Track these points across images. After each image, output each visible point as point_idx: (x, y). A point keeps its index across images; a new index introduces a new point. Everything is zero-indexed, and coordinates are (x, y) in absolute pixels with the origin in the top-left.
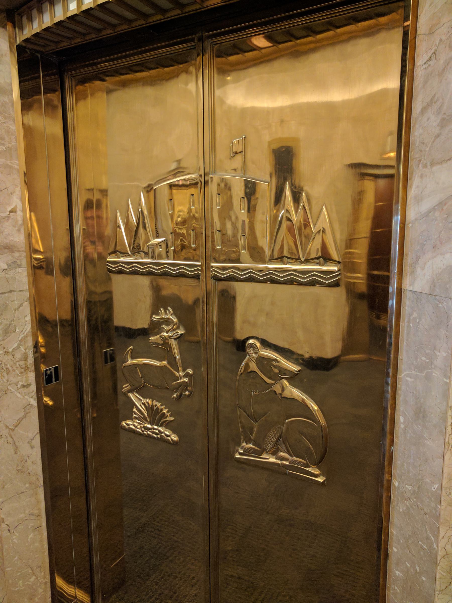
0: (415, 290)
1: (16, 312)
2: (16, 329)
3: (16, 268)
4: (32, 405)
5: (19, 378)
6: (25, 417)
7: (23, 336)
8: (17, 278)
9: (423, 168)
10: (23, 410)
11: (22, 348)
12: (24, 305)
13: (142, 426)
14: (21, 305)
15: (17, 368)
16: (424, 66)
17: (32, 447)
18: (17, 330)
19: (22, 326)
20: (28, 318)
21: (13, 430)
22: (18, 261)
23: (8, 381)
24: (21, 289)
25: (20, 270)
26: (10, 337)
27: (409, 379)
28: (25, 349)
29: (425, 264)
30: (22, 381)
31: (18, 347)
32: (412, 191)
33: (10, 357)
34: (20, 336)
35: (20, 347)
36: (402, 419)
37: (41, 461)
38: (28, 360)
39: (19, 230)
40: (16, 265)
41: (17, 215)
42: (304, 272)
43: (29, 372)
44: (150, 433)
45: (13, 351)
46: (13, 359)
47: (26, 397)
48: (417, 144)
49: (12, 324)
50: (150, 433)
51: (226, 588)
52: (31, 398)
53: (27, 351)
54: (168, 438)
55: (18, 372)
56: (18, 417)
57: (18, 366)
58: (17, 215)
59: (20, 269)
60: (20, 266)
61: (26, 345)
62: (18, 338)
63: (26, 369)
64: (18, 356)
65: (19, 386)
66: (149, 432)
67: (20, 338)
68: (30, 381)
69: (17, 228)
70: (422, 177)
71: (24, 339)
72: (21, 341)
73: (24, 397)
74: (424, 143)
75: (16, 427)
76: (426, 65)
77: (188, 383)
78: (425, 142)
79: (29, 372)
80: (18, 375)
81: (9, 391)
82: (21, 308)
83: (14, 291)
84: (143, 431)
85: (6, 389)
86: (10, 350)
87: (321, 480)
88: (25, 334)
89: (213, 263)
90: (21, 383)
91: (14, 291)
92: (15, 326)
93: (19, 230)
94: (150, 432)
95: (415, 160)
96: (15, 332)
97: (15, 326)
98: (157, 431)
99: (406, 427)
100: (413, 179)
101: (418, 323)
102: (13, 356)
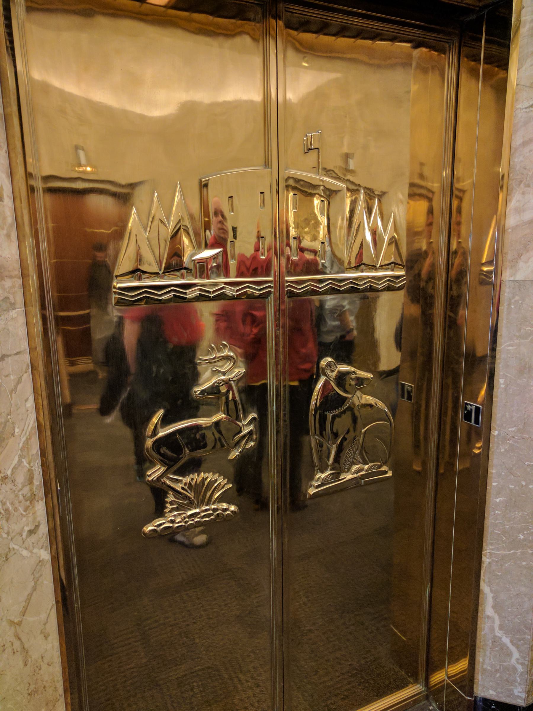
0: (516, 279)
1: (13, 395)
2: (14, 430)
3: (8, 310)
4: (43, 560)
5: (24, 519)
6: (34, 589)
7: (24, 439)
8: (10, 328)
9: (525, 187)
10: (33, 576)
11: (25, 462)
12: (23, 379)
13: (183, 516)
14: (19, 381)
15: (20, 502)
16: (525, 110)
17: (46, 637)
18: (17, 430)
19: (22, 420)
20: (31, 403)
21: (20, 624)
22: (11, 297)
23: (8, 533)
24: (17, 351)
25: (13, 313)
26: (8, 446)
27: (511, 348)
28: (29, 463)
29: (529, 259)
30: (27, 525)
31: (20, 462)
32: (512, 204)
33: (10, 485)
34: (20, 440)
35: (22, 462)
36: (502, 381)
37: (59, 653)
38: (34, 481)
39: (8, 236)
40: (8, 304)
41: (4, 206)
42: (380, 278)
43: (36, 503)
44: (199, 520)
45: (13, 473)
46: (14, 488)
47: (35, 551)
48: (517, 169)
49: (8, 421)
50: (199, 520)
51: (192, 690)
52: (42, 548)
53: (32, 464)
54: (227, 513)
55: (21, 510)
56: (26, 593)
57: (21, 498)
58: (4, 206)
59: (14, 311)
60: (13, 306)
61: (30, 454)
62: (19, 444)
63: (32, 498)
64: (20, 479)
65: (25, 534)
66: (196, 520)
67: (21, 445)
68: (38, 519)
69: (5, 232)
70: (523, 193)
71: (27, 443)
72: (22, 449)
73: (31, 552)
74: (525, 169)
75: (23, 615)
76: (528, 110)
77: (255, 430)
78: (527, 168)
79: (36, 503)
80: (22, 514)
81: (12, 552)
82: (20, 386)
83: (8, 356)
84: (186, 522)
85: (7, 550)
86: (9, 472)
87: (390, 474)
88: (28, 433)
89: (287, 277)
90: (27, 529)
91: (8, 356)
92: (13, 423)
93: (8, 236)
94: (199, 518)
95: (515, 180)
96: (13, 435)
97: (13, 423)
98: (211, 512)
99: (507, 386)
100: (512, 195)
101: (521, 303)
102: (13, 481)
